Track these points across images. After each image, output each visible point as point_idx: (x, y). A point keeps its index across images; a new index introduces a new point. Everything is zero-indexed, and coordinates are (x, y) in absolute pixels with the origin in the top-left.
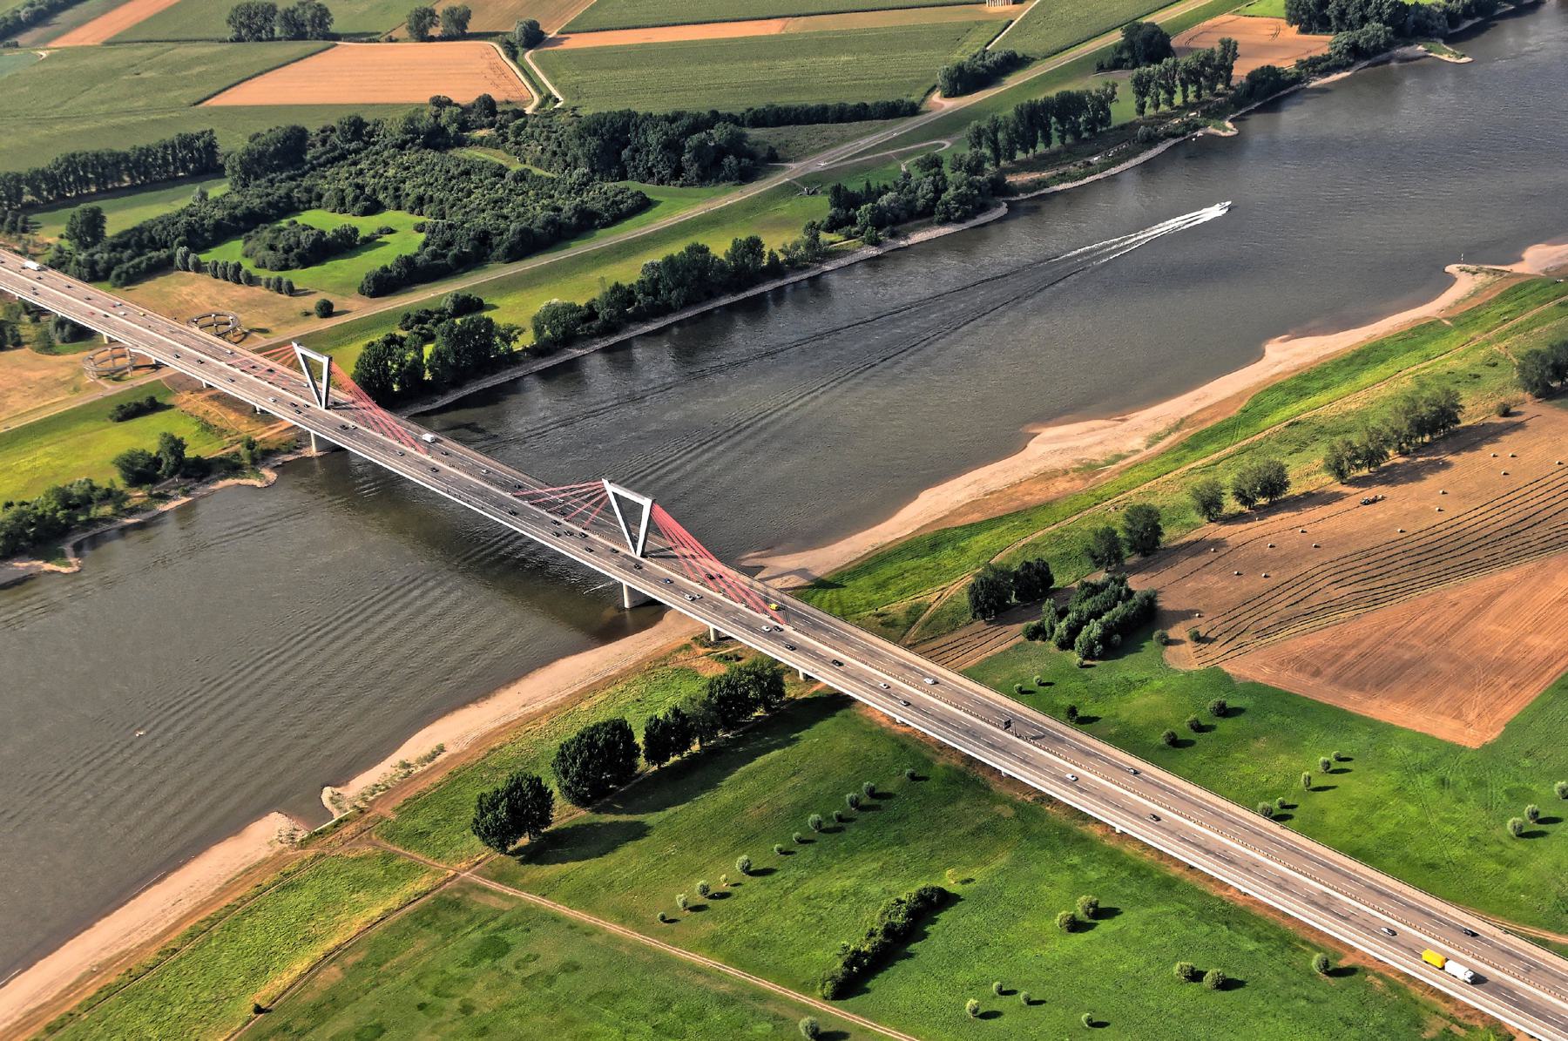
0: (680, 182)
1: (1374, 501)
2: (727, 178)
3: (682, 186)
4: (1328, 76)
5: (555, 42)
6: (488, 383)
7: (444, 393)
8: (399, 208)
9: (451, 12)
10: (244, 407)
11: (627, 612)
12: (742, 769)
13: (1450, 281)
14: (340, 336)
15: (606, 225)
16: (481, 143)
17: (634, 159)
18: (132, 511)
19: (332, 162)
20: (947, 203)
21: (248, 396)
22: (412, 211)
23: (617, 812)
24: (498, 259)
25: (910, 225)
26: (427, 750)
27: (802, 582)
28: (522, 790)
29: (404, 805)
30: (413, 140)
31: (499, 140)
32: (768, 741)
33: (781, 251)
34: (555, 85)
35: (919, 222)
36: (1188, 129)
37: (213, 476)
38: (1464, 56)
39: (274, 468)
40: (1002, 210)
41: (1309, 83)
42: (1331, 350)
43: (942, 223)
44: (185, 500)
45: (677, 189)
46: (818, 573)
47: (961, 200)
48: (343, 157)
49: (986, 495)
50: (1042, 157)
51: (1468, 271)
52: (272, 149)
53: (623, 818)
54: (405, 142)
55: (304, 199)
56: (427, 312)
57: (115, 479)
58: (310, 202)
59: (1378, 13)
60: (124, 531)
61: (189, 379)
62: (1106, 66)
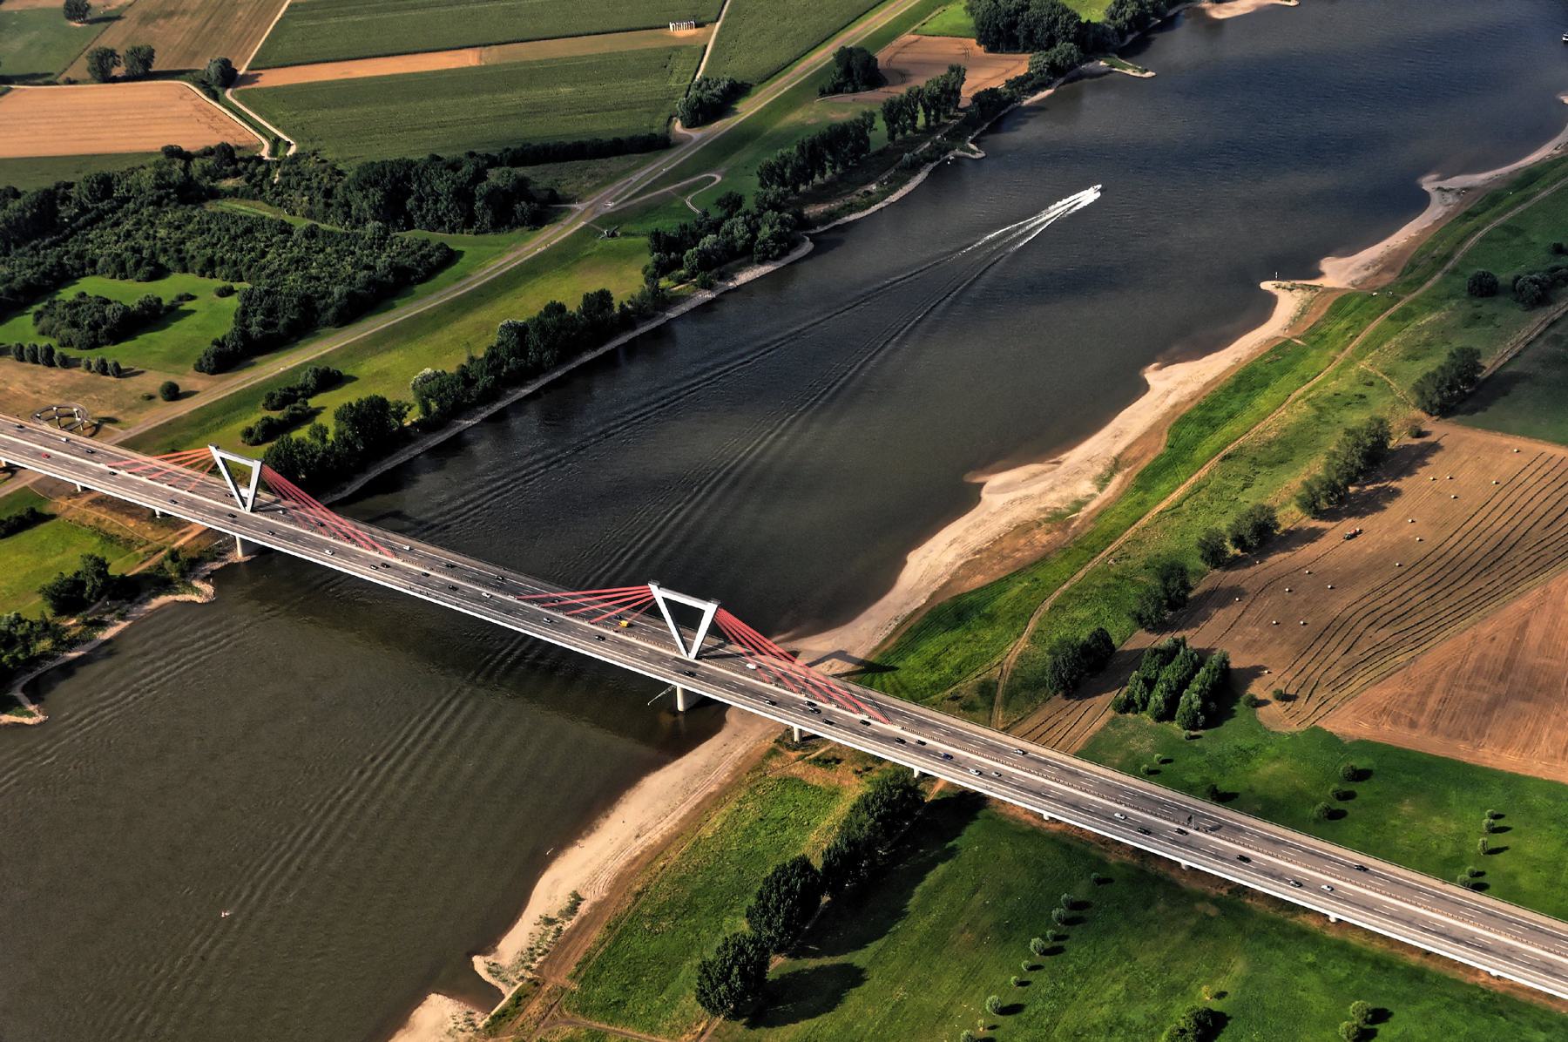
0: (474, 229)
1: (1354, 535)
2: (519, 224)
3: (476, 234)
4: (1035, 94)
5: (247, 79)
6: (389, 464)
7: (350, 479)
8: (185, 270)
9: (135, 52)
10: (137, 511)
11: (681, 718)
12: (918, 889)
13: (1270, 301)
14: (201, 423)
15: (422, 281)
16: (234, 193)
17: (420, 208)
18: (72, 644)
19: (91, 223)
20: (764, 242)
21: (187, 513)
22: (202, 274)
23: (816, 955)
24: (327, 324)
25: (731, 265)
26: (563, 901)
27: (848, 667)
28: (747, 955)
29: (579, 971)
30: (168, 195)
31: (256, 190)
32: (924, 855)
33: (629, 302)
34: (277, 127)
35: (739, 261)
36: (940, 153)
37: (146, 595)
38: (1146, 71)
39: (205, 579)
40: (808, 246)
41: (1022, 102)
42: (1209, 377)
43: (761, 262)
44: (123, 625)
45: (471, 237)
46: (859, 653)
47: (777, 238)
48: (100, 217)
49: (975, 554)
50: (823, 187)
51: (1284, 288)
52: (28, 214)
53: (827, 961)
54: (161, 198)
55: (77, 266)
56: (290, 389)
57: (36, 608)
58: (83, 268)
59: (1064, 33)
60: (69, 669)
61: (60, 483)
62: (827, 90)
